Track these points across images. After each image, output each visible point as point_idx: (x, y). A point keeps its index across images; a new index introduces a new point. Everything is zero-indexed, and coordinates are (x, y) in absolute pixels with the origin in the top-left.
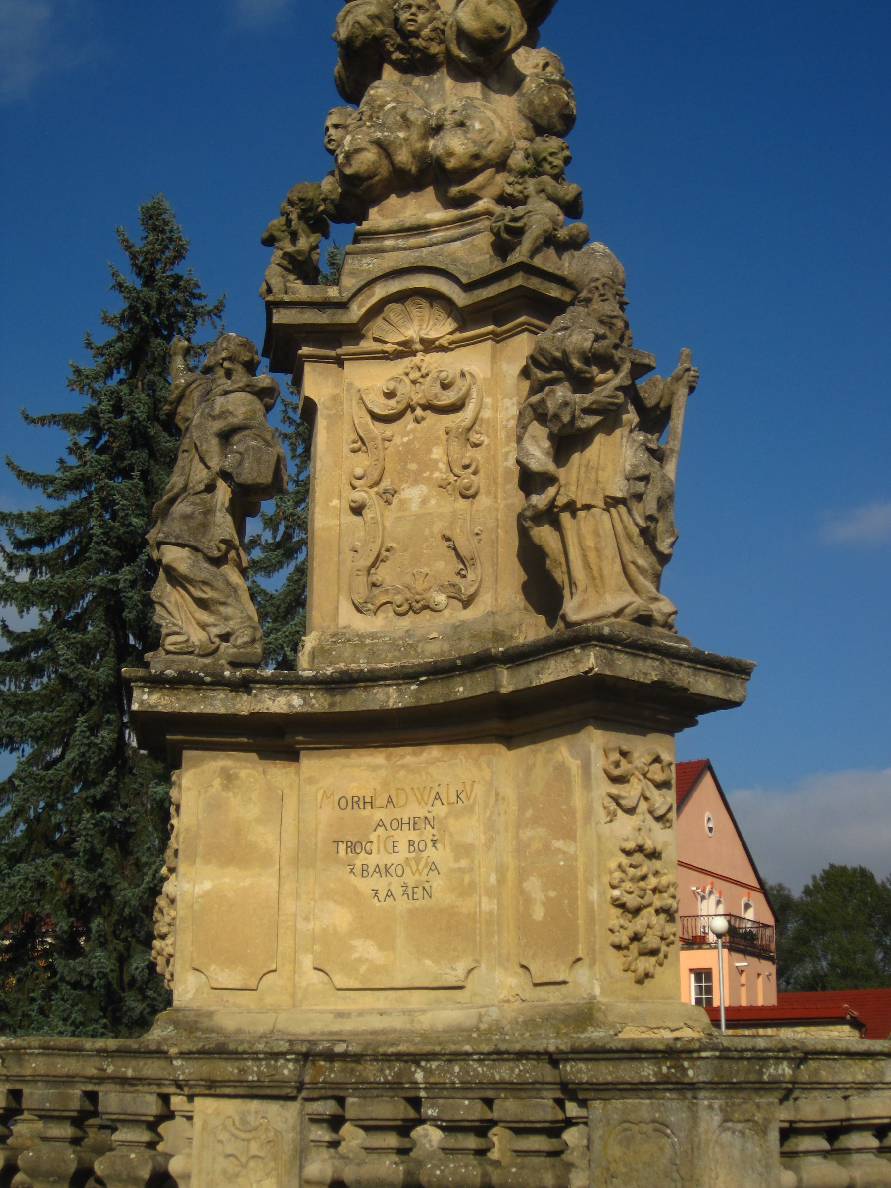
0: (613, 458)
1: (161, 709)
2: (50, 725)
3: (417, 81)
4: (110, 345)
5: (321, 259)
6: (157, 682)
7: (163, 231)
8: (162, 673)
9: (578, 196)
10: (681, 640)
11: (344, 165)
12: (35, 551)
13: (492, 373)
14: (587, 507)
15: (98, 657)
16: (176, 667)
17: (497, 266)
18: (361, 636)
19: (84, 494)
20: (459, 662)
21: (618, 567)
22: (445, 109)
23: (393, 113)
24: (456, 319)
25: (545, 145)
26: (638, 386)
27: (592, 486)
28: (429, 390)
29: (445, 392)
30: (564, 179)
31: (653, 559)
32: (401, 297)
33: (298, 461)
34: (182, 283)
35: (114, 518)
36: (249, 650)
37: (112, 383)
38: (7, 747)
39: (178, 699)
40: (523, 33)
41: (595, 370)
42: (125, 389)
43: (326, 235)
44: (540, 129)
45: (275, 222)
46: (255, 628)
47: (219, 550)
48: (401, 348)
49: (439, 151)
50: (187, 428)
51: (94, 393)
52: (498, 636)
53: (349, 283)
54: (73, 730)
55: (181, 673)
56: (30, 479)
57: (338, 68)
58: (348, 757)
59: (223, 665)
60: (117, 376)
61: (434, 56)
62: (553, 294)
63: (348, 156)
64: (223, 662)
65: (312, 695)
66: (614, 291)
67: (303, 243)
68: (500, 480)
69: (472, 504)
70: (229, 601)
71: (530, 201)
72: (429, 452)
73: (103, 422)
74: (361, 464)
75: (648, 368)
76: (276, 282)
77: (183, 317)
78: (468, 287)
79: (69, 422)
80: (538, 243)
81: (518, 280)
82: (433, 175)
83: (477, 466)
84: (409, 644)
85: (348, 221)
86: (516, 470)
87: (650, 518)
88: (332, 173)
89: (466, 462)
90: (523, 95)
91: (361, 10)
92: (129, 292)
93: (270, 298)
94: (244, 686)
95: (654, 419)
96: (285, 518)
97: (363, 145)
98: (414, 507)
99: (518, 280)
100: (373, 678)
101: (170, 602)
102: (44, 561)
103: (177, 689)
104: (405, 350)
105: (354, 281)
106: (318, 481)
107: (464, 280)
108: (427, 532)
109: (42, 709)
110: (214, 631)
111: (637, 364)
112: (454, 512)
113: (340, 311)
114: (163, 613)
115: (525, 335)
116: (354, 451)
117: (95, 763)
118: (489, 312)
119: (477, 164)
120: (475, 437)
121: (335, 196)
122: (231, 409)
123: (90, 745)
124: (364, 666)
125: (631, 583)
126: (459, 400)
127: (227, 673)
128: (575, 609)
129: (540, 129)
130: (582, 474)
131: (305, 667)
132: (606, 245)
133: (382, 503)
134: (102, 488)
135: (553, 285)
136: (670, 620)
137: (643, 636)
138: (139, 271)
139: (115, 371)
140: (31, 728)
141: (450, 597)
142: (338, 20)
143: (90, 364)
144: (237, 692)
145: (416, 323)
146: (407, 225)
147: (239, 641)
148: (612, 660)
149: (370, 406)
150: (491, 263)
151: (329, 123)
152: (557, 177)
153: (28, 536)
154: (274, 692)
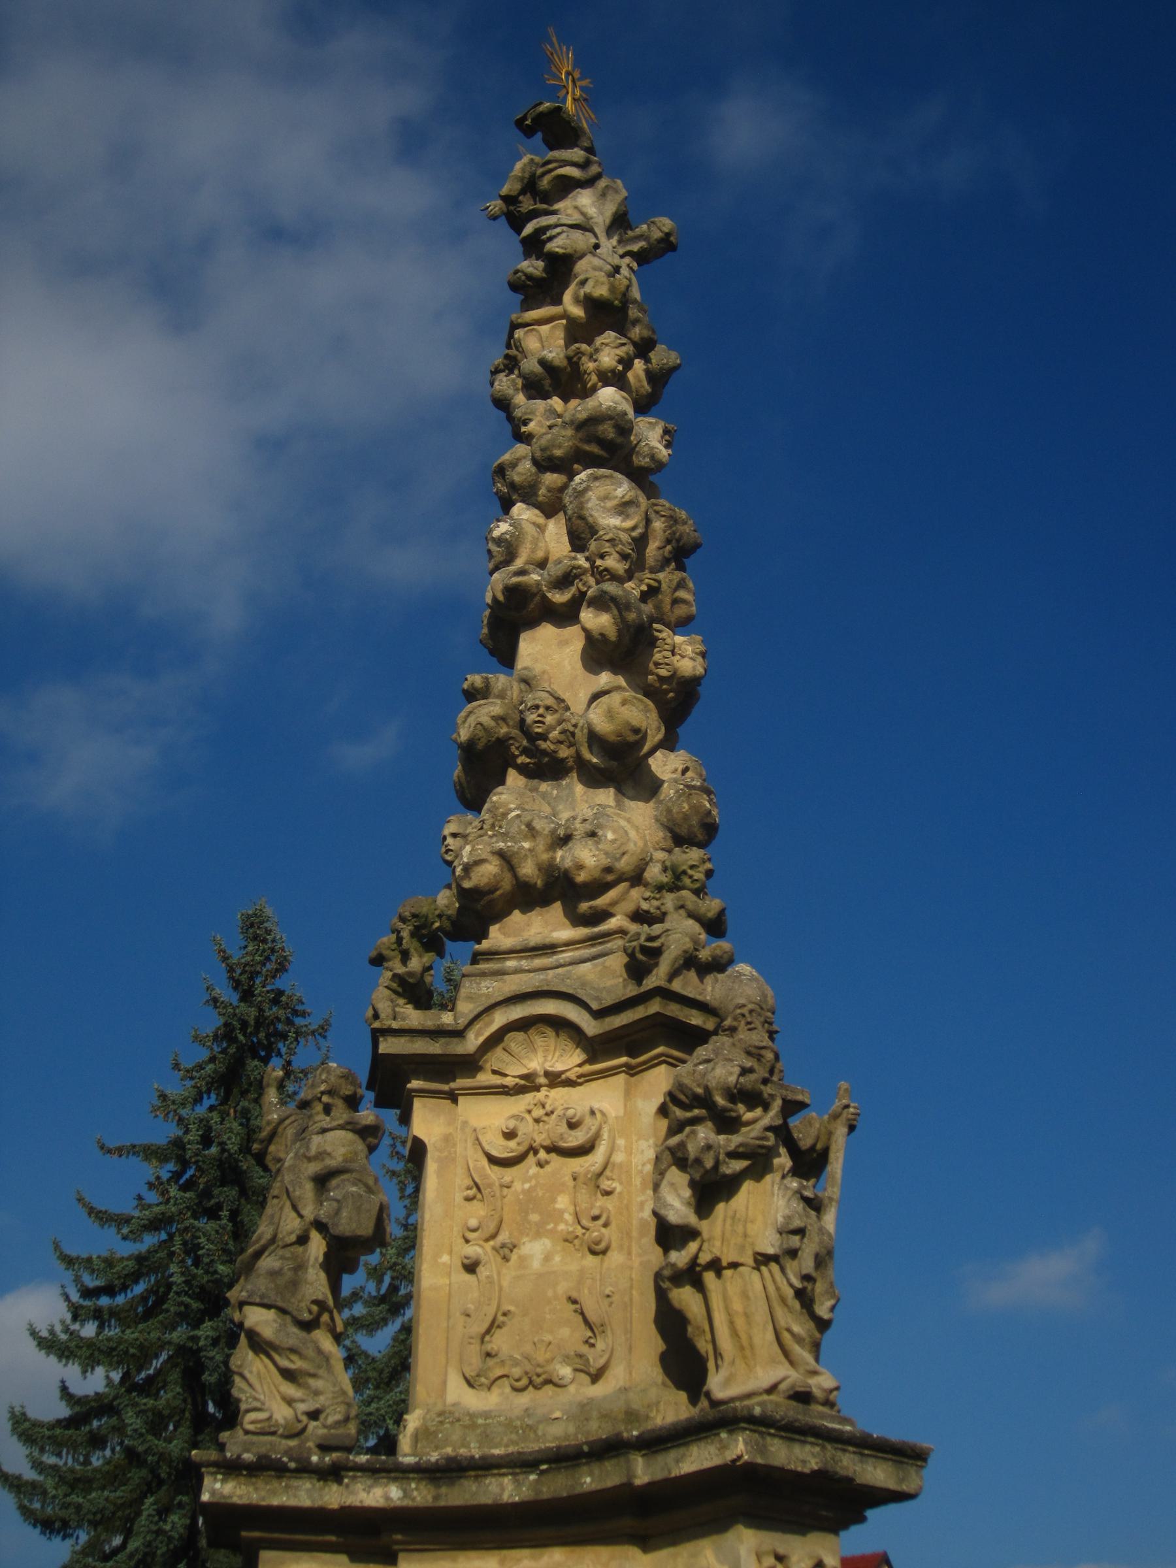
0: (762, 1209)
1: (235, 1500)
2: (112, 1508)
3: (544, 787)
4: (200, 1067)
5: (437, 981)
6: (232, 1468)
7: (264, 941)
8: (239, 1457)
9: (722, 912)
10: (845, 1420)
11: (462, 878)
12: (104, 1301)
13: (625, 1111)
14: (734, 1265)
15: (171, 1427)
16: (254, 1450)
17: (632, 990)
18: (472, 1416)
19: (164, 1236)
20: (586, 1448)
21: (770, 1335)
22: (574, 818)
23: (518, 821)
24: (585, 1050)
25: (685, 856)
26: (791, 1125)
27: (740, 1240)
28: (554, 1130)
29: (573, 1133)
30: (706, 894)
31: (811, 1325)
32: (523, 1025)
33: (407, 1202)
34: (284, 999)
35: (197, 1263)
36: (341, 1431)
37: (201, 1110)
38: (58, 1533)
39: (256, 1489)
40: (660, 736)
41: (741, 1108)
42: (215, 1116)
43: (441, 954)
44: (680, 840)
45: (385, 939)
46: (349, 1405)
47: (310, 1312)
48: (523, 1082)
49: (568, 863)
50: (279, 1170)
51: (181, 1120)
52: (631, 1416)
53: (466, 1008)
54: (138, 1513)
55: (261, 1457)
56: (103, 1217)
57: (458, 772)
58: (454, 1560)
59: (310, 1449)
60: (207, 1103)
61: (563, 760)
62: (694, 1022)
63: (467, 869)
64: (310, 1444)
65: (413, 1485)
66: (762, 1019)
67: (415, 964)
68: (635, 1234)
69: (602, 1261)
70: (321, 1372)
71: (668, 918)
72: (553, 1200)
73: (189, 1154)
74: (476, 1213)
75: (802, 1106)
76: (384, 1007)
77: (284, 1036)
78: (599, 1014)
79: (149, 1153)
80: (677, 965)
81: (655, 1007)
82: (562, 889)
83: (608, 1217)
84: (527, 1425)
85: (465, 940)
86: (653, 1222)
87: (807, 1278)
88: (449, 887)
89: (596, 1212)
90: (661, 802)
91: (485, 710)
92: (225, 1007)
93: (376, 1025)
94: (334, 1474)
95: (810, 1163)
96: (391, 1268)
97: (483, 857)
98: (536, 1264)
99: (655, 1007)
100: (485, 1466)
101: (251, 1372)
102: (113, 1313)
103: (256, 1476)
104: (528, 1084)
105: (471, 1006)
106: (426, 1233)
107: (595, 1006)
108: (550, 1293)
109: (103, 1488)
110: (302, 1407)
111: (790, 1101)
112: (582, 1271)
113: (455, 1040)
114: (243, 1385)
115: (663, 1068)
116: (469, 1199)
117: (163, 1555)
118: (621, 1043)
119: (610, 878)
120: (606, 1184)
121: (452, 912)
122: (329, 1149)
123: (159, 1532)
124: (475, 1451)
125: (786, 1353)
126: (587, 1142)
127: (315, 1459)
128: (721, 1384)
129: (680, 840)
130: (728, 1227)
131: (406, 1455)
132: (753, 966)
133: (499, 1259)
134: (186, 1229)
135: (694, 1012)
136: (832, 1397)
137: (800, 1417)
138: (237, 985)
139: (205, 1096)
140: (89, 1511)
141: (576, 1370)
142: (459, 721)
143: (177, 1089)
144: (326, 1480)
145: (540, 1054)
146: (532, 944)
147: (330, 1420)
148: (765, 1446)
149: (487, 1148)
150: (625, 987)
151: (446, 832)
152: (697, 892)
153: (98, 1283)
154: (369, 1482)
